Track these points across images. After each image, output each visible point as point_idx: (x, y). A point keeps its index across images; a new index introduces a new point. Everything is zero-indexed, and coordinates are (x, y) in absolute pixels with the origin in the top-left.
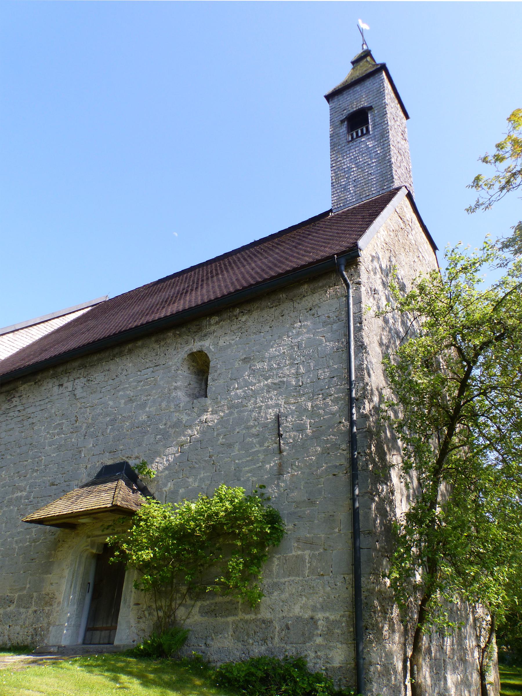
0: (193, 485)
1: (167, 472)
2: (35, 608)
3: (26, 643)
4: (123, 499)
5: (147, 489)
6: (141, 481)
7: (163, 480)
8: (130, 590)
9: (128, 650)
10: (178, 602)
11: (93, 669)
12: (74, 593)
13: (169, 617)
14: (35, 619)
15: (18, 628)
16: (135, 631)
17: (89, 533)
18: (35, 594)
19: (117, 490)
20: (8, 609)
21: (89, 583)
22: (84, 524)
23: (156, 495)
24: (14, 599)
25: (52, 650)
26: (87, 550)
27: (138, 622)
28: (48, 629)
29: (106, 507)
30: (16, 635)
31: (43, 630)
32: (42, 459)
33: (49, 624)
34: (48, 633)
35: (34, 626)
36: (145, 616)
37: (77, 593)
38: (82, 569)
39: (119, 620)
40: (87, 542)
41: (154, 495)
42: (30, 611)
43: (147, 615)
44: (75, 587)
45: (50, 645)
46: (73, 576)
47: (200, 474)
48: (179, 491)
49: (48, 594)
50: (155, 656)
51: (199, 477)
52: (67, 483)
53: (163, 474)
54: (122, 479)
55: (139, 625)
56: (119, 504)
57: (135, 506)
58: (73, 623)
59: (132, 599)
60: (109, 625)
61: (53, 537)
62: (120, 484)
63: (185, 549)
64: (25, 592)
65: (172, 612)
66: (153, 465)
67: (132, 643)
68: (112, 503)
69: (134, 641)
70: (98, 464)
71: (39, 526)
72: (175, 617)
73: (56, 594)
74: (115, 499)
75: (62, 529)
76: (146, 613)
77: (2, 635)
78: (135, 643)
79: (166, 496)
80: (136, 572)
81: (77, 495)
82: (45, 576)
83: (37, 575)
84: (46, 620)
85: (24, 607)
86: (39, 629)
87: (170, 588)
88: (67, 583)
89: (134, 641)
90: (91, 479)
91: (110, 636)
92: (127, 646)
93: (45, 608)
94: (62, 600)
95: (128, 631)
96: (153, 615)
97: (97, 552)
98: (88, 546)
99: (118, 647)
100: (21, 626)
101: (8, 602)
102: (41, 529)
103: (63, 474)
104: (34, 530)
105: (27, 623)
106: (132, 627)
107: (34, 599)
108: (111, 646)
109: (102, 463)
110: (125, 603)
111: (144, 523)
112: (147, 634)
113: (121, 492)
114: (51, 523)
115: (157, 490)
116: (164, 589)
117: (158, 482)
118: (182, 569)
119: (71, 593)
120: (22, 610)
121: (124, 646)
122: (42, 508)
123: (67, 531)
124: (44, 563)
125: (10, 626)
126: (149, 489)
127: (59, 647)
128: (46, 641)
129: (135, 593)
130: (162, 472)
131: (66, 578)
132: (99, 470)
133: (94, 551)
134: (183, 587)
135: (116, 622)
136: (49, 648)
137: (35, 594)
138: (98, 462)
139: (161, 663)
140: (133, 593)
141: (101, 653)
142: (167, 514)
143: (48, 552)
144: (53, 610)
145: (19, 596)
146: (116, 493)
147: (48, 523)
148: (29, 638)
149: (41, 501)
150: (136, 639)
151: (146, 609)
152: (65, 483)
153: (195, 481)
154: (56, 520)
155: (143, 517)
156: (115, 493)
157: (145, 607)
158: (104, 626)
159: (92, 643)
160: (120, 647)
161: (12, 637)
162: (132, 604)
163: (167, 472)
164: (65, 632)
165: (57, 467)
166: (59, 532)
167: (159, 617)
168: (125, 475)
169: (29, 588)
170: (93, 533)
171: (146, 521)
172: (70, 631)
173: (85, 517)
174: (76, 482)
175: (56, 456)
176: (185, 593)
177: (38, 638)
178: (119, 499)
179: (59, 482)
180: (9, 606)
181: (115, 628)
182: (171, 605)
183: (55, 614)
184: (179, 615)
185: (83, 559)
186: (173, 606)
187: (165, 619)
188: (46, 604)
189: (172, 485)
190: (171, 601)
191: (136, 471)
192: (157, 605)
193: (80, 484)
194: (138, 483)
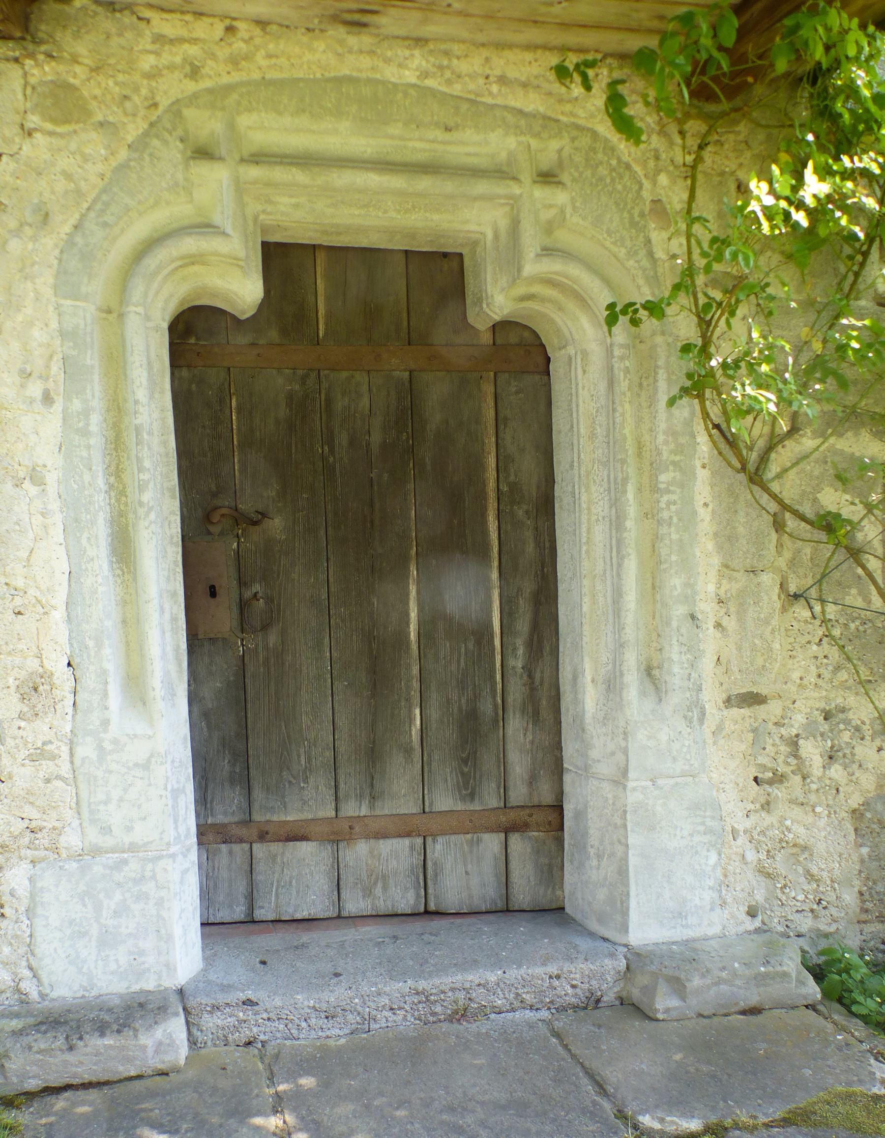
8: (679, 611)
59: (707, 663)
60: (408, 806)
129: (718, 625)
150: (759, 897)
170: (244, 121)
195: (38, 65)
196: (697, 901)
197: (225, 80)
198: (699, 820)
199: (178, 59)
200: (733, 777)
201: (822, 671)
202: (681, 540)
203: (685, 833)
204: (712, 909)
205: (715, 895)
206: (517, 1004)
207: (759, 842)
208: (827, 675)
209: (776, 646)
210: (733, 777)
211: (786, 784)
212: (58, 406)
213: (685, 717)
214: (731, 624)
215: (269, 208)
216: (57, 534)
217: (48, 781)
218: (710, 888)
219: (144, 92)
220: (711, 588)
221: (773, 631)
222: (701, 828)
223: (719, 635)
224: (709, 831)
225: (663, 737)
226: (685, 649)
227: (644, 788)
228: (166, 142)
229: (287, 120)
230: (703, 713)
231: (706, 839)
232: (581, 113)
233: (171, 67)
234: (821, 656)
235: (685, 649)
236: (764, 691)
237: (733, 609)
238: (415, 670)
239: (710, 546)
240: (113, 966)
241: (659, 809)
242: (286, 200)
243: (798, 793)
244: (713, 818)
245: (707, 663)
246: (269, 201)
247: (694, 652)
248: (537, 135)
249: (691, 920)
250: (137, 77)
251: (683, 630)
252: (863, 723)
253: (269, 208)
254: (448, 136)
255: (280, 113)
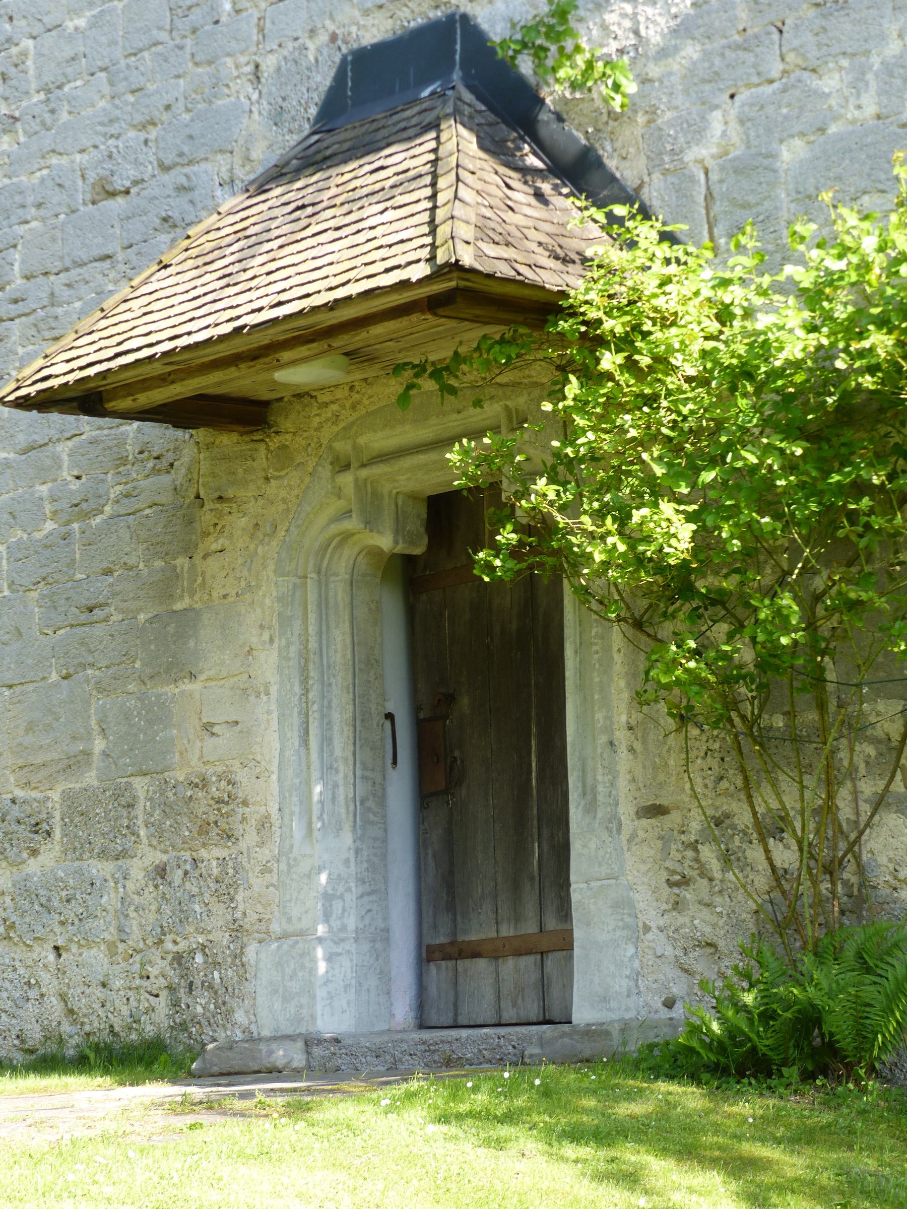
0: (851, 113)
1: (691, 51)
2: (160, 857)
3: (150, 1031)
4: (483, 231)
5: (599, 163)
6: (560, 119)
7: (679, 100)
8: (603, 739)
9: (651, 1047)
10: (869, 787)
11: (504, 1131)
12: (328, 768)
13: (831, 869)
14: (167, 909)
15: (97, 957)
16: (669, 951)
17: (343, 447)
18: (140, 785)
19: (442, 183)
20: (33, 866)
21: (390, 717)
22: (303, 395)
23: (652, 195)
24: (50, 816)
25: (280, 1055)
26: (346, 537)
27: (677, 905)
28: (238, 956)
29: (405, 284)
30: (99, 992)
31: (216, 964)
32: (24, 54)
33: (237, 930)
34: (243, 979)
35: (169, 946)
36: (704, 872)
37: (344, 770)
38: (340, 636)
39: (575, 897)
40: (338, 493)
41: (645, 194)
42: (138, 869)
43: (715, 866)
44: (326, 741)
45: (266, 1033)
46: (305, 681)
47: (883, 38)
48: (772, 156)
49: (204, 783)
50: (792, 1073)
51: (875, 61)
52: (176, 177)
53: (677, 64)
54: (456, 114)
55: (681, 920)
56: (467, 258)
57: (557, 265)
58: (351, 922)
59: (623, 783)
60: (530, 927)
61: (165, 480)
62: (451, 146)
63: (860, 488)
64: (91, 778)
65: (843, 845)
66: (610, 18)
67: (665, 1013)
68: (432, 259)
69: (669, 1004)
70: (311, 46)
71: (87, 424)
72: (861, 869)
73: (241, 776)
74: (443, 231)
75: (201, 434)
76: (708, 853)
77: (33, 994)
78: (678, 1011)
79: (709, 196)
80: (617, 636)
81: (240, 234)
82: (170, 689)
83: (131, 687)
84: (220, 915)
85: (103, 854)
86: (199, 958)
87: (812, 716)
88: (282, 718)
89: (669, 1004)
90: (295, 138)
91: (543, 985)
92: (643, 1025)
93: (203, 853)
94: (273, 809)
95: (631, 950)
96: (745, 865)
97: (400, 548)
98: (347, 514)
99: (590, 1033)
100: (112, 949)
101: (22, 831)
102: (93, 442)
103: (143, 127)
104: (63, 449)
105: (135, 933)
106: (647, 929)
107: (139, 811)
108: (566, 1028)
109: (334, 38)
110: (591, 807)
111: (620, 358)
112: (731, 961)
113: (463, 192)
114: (145, 399)
115: (655, 162)
116: (779, 722)
117: (652, 112)
118: (859, 603)
119: (315, 774)
120: (99, 868)
121: (625, 1028)
122: (84, 326)
123: (228, 440)
124: (150, 621)
125: (56, 948)
126: (611, 163)
127: (310, 1042)
128: (240, 1017)
129: (631, 750)
130: (663, 53)
131: (274, 689)
132: (324, 79)
133: (385, 542)
134: (881, 706)
135: (564, 911)
136: (263, 1047)
137: (140, 785)
138: (313, 32)
139: (832, 1102)
140: (623, 753)
141: (520, 1061)
142: (735, 295)
143: (159, 564)
144: (243, 859)
145: (67, 796)
146: (441, 198)
147: (125, 404)
148: (162, 1004)
149: (66, 293)
150: (677, 990)
151: (707, 836)
152: (166, 178)
153: (858, 84)
154: (163, 380)
155: (608, 324)
156: (433, 197)
157: (695, 826)
158: (507, 931)
159: (462, 1020)
160: (608, 1033)
161: (80, 1004)
162: (626, 811)
163: (691, 51)
164: (322, 967)
165: (106, 89)
166: (188, 453)
167: (777, 875)
168: (468, 96)
169: (105, 754)
170: (362, 440)
171: (625, 343)
172: (346, 965)
173: (303, 351)
174: (220, 165)
175: (92, 25)
176: (896, 737)
177: (200, 1004)
178: (465, 231)
179: (133, 173)
180: (34, 853)
181: (566, 944)
182: (828, 809)
183: (257, 883)
184: (883, 860)
185: (339, 591)
186: (845, 812)
187: (815, 883)
188: (204, 829)
189: (734, 124)
190: (830, 784)
191: (526, 66)
192: (760, 810)
193: (245, 175)
194: (544, 132)
195: (272, 441)
196: (617, 988)
197: (351, 419)
198: (619, 917)
199: (329, 415)
200: (646, 880)
201: (707, 781)
202: (601, 682)
203: (610, 928)
204: (628, 996)
205: (632, 984)
206: (482, 1060)
207: (675, 939)
208: (711, 785)
209: (672, 762)
210: (646, 880)
211: (692, 886)
212: (276, 645)
213: (607, 828)
214: (638, 746)
215: (396, 485)
216: (275, 725)
217: (267, 887)
218: (627, 977)
219: (315, 440)
220: (624, 718)
221: (669, 751)
222: (621, 924)
223: (631, 757)
224: (626, 927)
225: (593, 845)
226: (607, 771)
227: (581, 889)
228: (324, 467)
229: (380, 434)
230: (620, 824)
231: (625, 933)
232: (533, 373)
233: (328, 420)
234: (706, 768)
235: (607, 771)
236: (664, 801)
237: (639, 735)
238: (535, 812)
239: (622, 683)
240: (288, 1015)
241: (592, 907)
242: (401, 477)
243: (705, 895)
244: (629, 915)
245: (623, 783)
246: (395, 481)
247: (612, 771)
248: (507, 399)
249: (613, 1004)
250: (312, 432)
251: (605, 755)
252: (746, 826)
253: (396, 485)
254: (461, 415)
255: (375, 431)
